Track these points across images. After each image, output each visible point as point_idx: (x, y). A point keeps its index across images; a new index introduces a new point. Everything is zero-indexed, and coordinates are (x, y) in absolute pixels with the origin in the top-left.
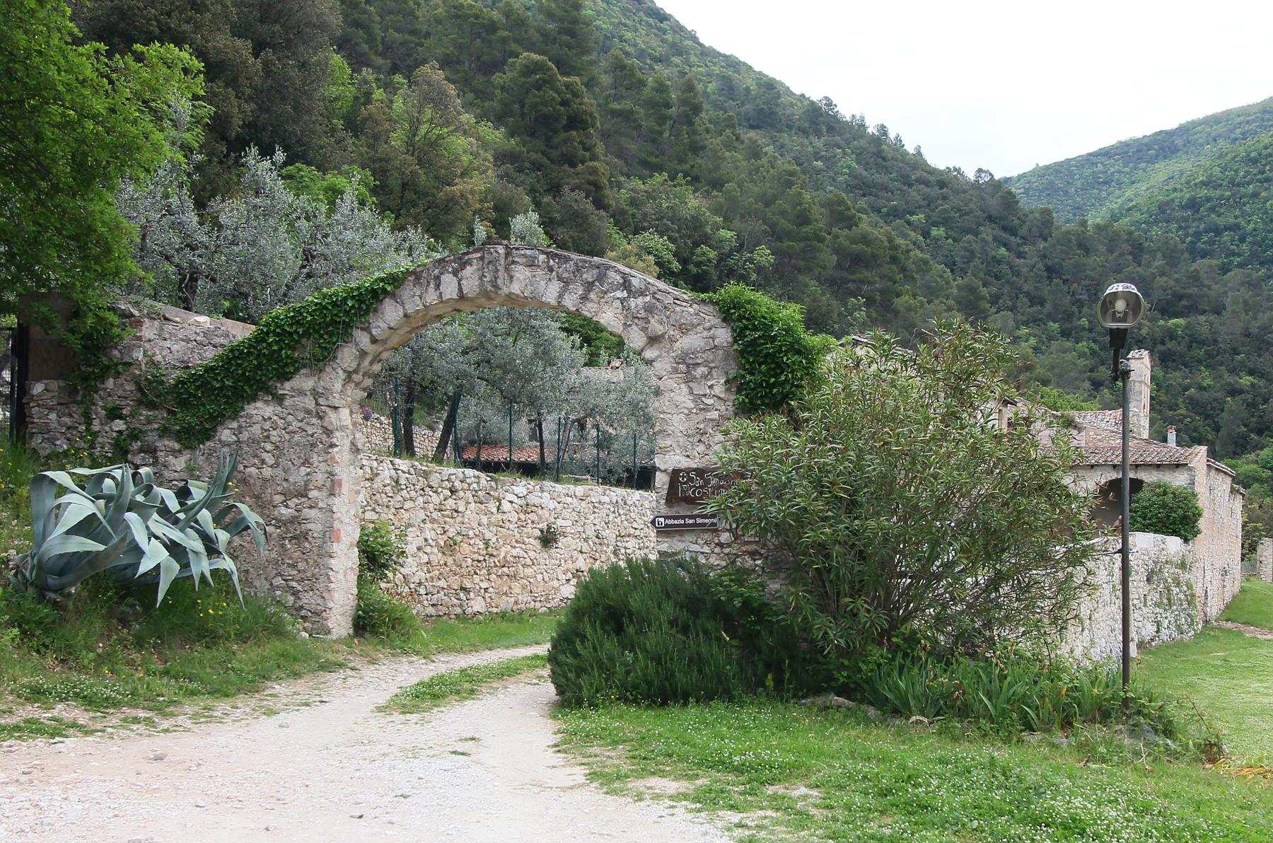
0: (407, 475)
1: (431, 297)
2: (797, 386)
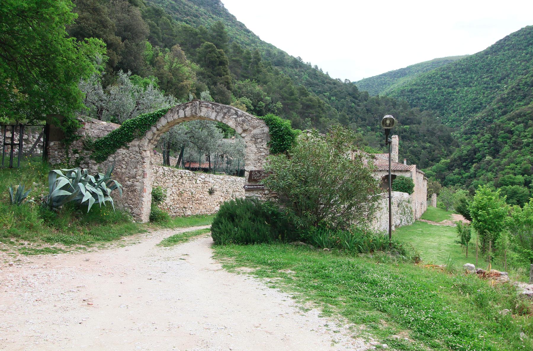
1: (176, 117)
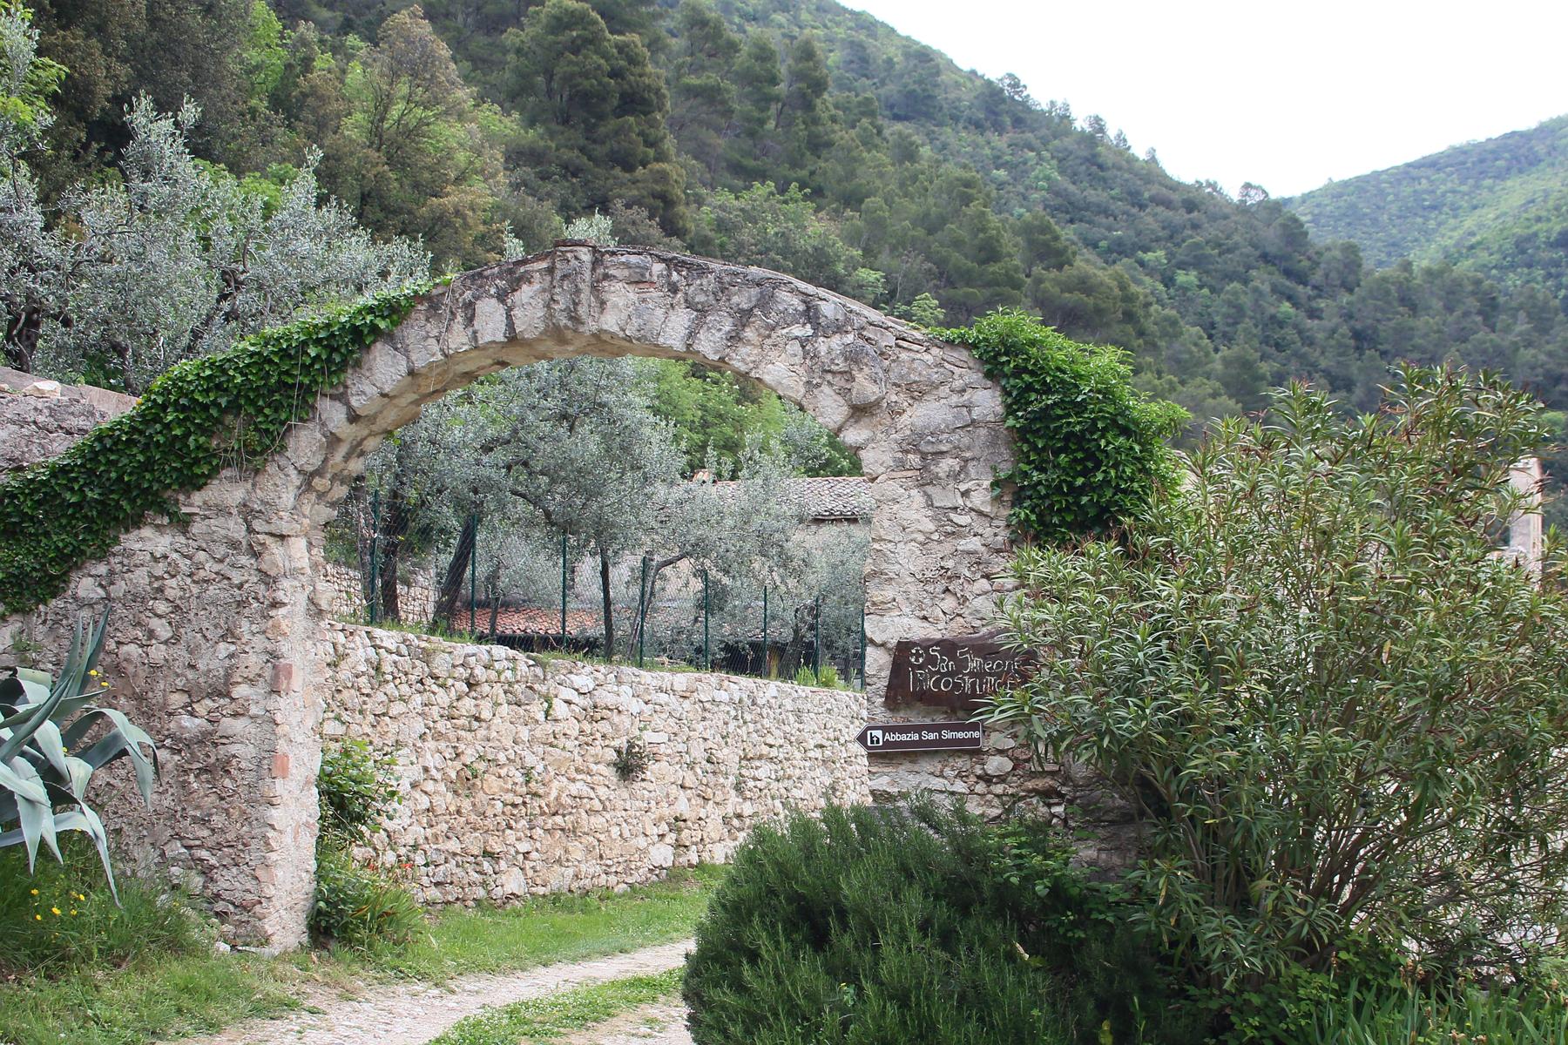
0: (395, 657)
1: (458, 339)
2: (1124, 491)
